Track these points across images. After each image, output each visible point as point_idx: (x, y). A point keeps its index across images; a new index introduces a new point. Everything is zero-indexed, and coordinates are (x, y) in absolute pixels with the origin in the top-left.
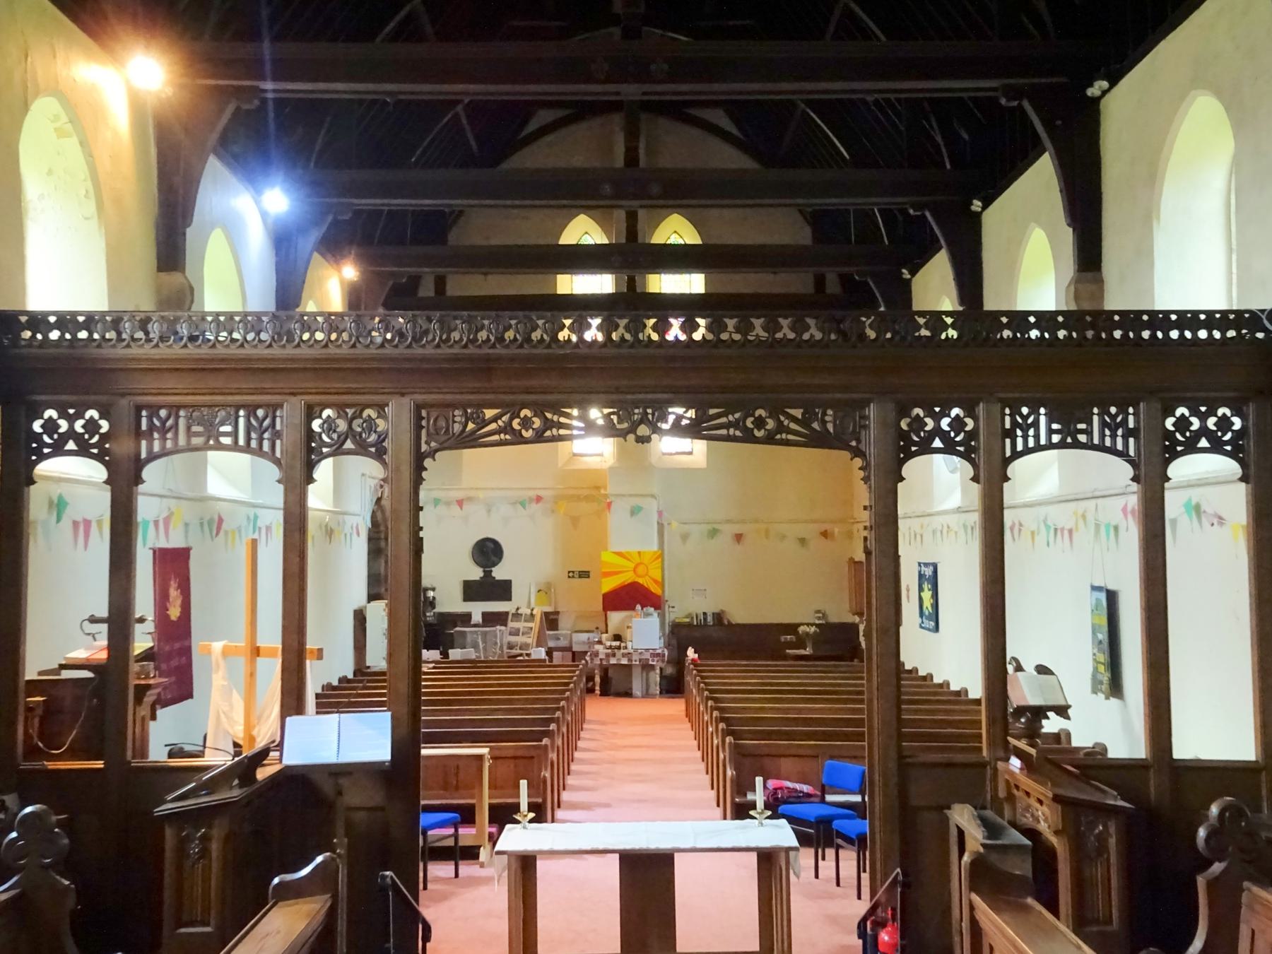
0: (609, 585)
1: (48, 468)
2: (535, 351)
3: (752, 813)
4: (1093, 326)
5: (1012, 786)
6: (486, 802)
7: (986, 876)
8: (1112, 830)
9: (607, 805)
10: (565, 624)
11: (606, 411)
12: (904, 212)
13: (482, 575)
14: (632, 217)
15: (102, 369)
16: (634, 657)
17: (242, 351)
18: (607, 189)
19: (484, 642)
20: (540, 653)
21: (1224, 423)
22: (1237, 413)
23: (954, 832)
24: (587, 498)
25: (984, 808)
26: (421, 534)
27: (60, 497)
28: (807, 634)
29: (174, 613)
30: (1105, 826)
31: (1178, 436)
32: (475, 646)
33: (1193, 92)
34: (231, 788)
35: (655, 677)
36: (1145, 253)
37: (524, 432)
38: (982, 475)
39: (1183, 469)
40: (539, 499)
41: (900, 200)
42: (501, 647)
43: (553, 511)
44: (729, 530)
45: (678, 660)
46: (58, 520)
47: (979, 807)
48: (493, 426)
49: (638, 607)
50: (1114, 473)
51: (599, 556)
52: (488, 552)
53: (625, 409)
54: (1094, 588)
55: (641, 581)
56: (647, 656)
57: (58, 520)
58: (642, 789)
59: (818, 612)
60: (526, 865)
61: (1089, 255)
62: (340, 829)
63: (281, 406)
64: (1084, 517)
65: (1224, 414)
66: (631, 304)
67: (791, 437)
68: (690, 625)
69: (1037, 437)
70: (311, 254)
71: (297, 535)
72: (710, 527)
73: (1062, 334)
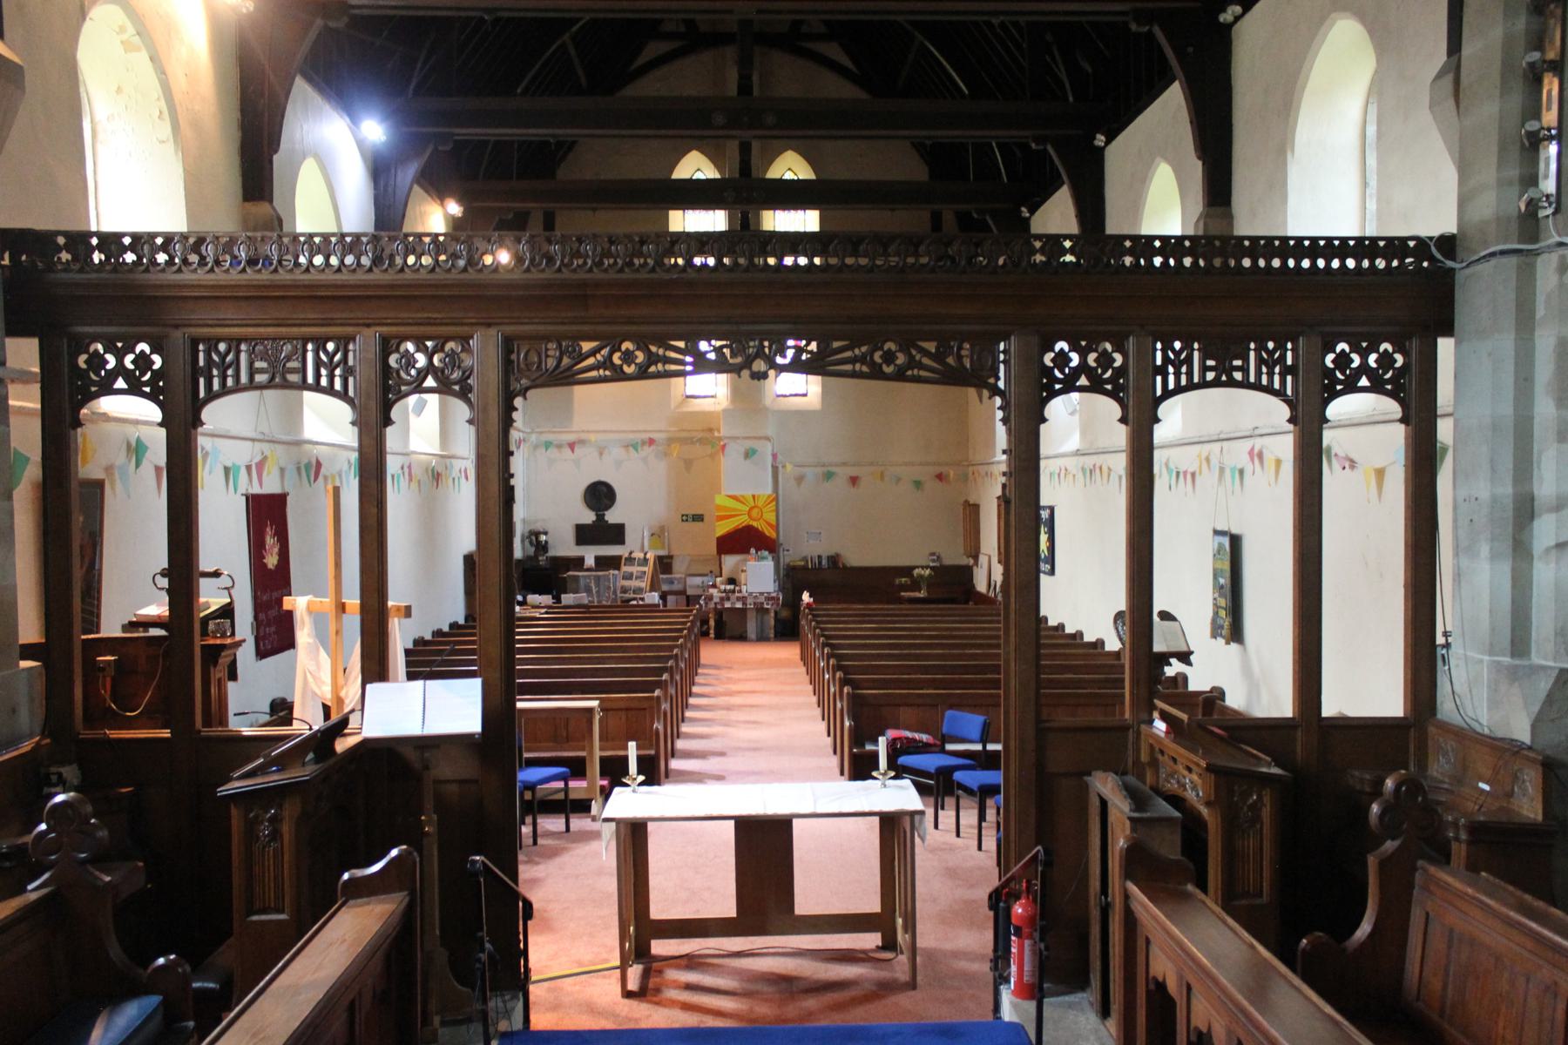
0: (723, 528)
1: (108, 404)
2: (638, 276)
3: (874, 774)
5: (1156, 750)
6: (598, 754)
7: (1140, 863)
8: (1267, 800)
9: (722, 754)
10: (679, 568)
11: (718, 343)
12: (1025, 147)
14: (745, 149)
15: (150, 298)
17: (306, 277)
18: (719, 119)
19: (598, 585)
20: (653, 598)
22: (1400, 348)
23: (1095, 803)
24: (701, 441)
25: (1124, 773)
26: (513, 482)
27: (138, 440)
28: (921, 576)
29: (272, 561)
30: (1260, 797)
32: (588, 590)
33: (1333, 15)
34: (304, 764)
35: (771, 621)
36: (1278, 185)
37: (625, 368)
38: (1131, 416)
39: (1340, 408)
40: (651, 442)
41: (1022, 133)
42: (615, 592)
43: (666, 454)
44: (844, 473)
45: (793, 602)
46: (137, 466)
47: (1121, 772)
48: (591, 361)
49: (753, 551)
50: (1267, 413)
52: (600, 495)
53: (739, 341)
54: (1217, 533)
55: (755, 524)
56: (762, 599)
57: (137, 466)
58: (761, 751)
60: (634, 834)
61: (1218, 189)
62: (429, 804)
63: (354, 339)
64: (1208, 460)
66: (745, 237)
67: (923, 373)
68: (805, 568)
69: (1190, 374)
70: (411, 188)
71: (373, 484)
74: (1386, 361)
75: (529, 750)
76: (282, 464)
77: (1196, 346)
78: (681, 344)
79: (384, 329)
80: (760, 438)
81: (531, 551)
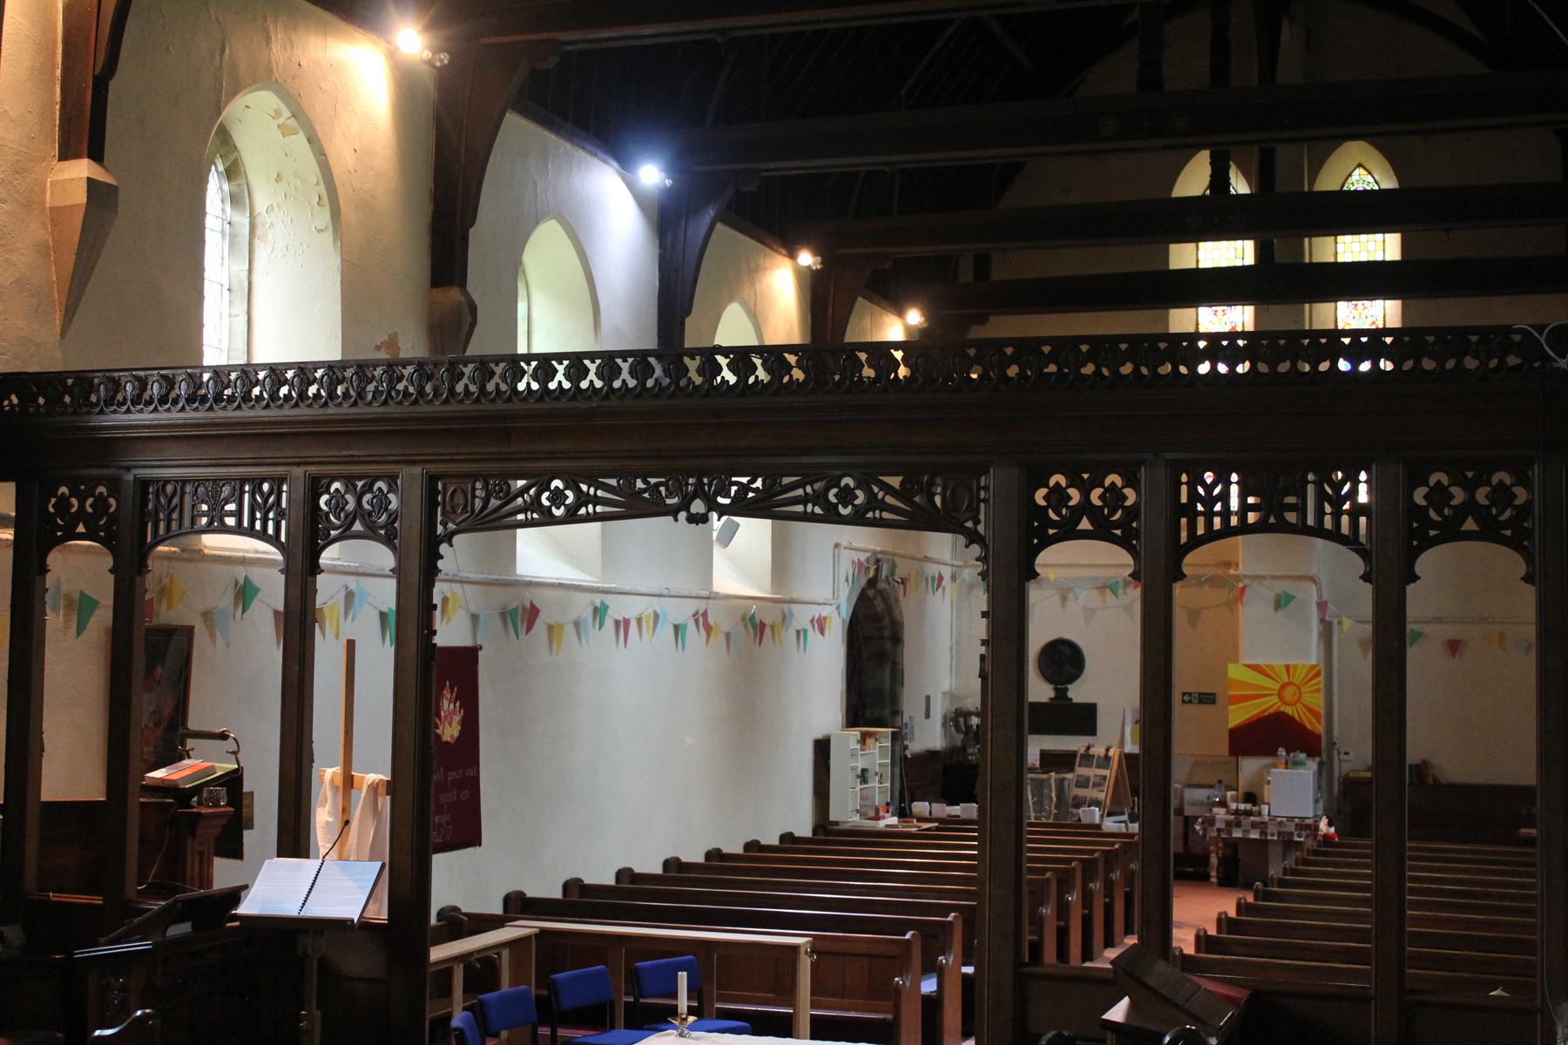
0: (1238, 715)
4: (1130, 356)
13: (1052, 694)
21: (1502, 495)
27: (246, 578)
29: (450, 731)
31: (1433, 514)
49: (1282, 752)
51: (1225, 671)
55: (1289, 710)
56: (1291, 828)
65: (1439, 483)
67: (886, 515)
73: (1127, 369)
74: (1502, 495)
75: (721, 999)
76: (473, 608)
77: (1234, 477)
78: (613, 482)
79: (312, 469)
80: (1299, 578)
81: (959, 739)
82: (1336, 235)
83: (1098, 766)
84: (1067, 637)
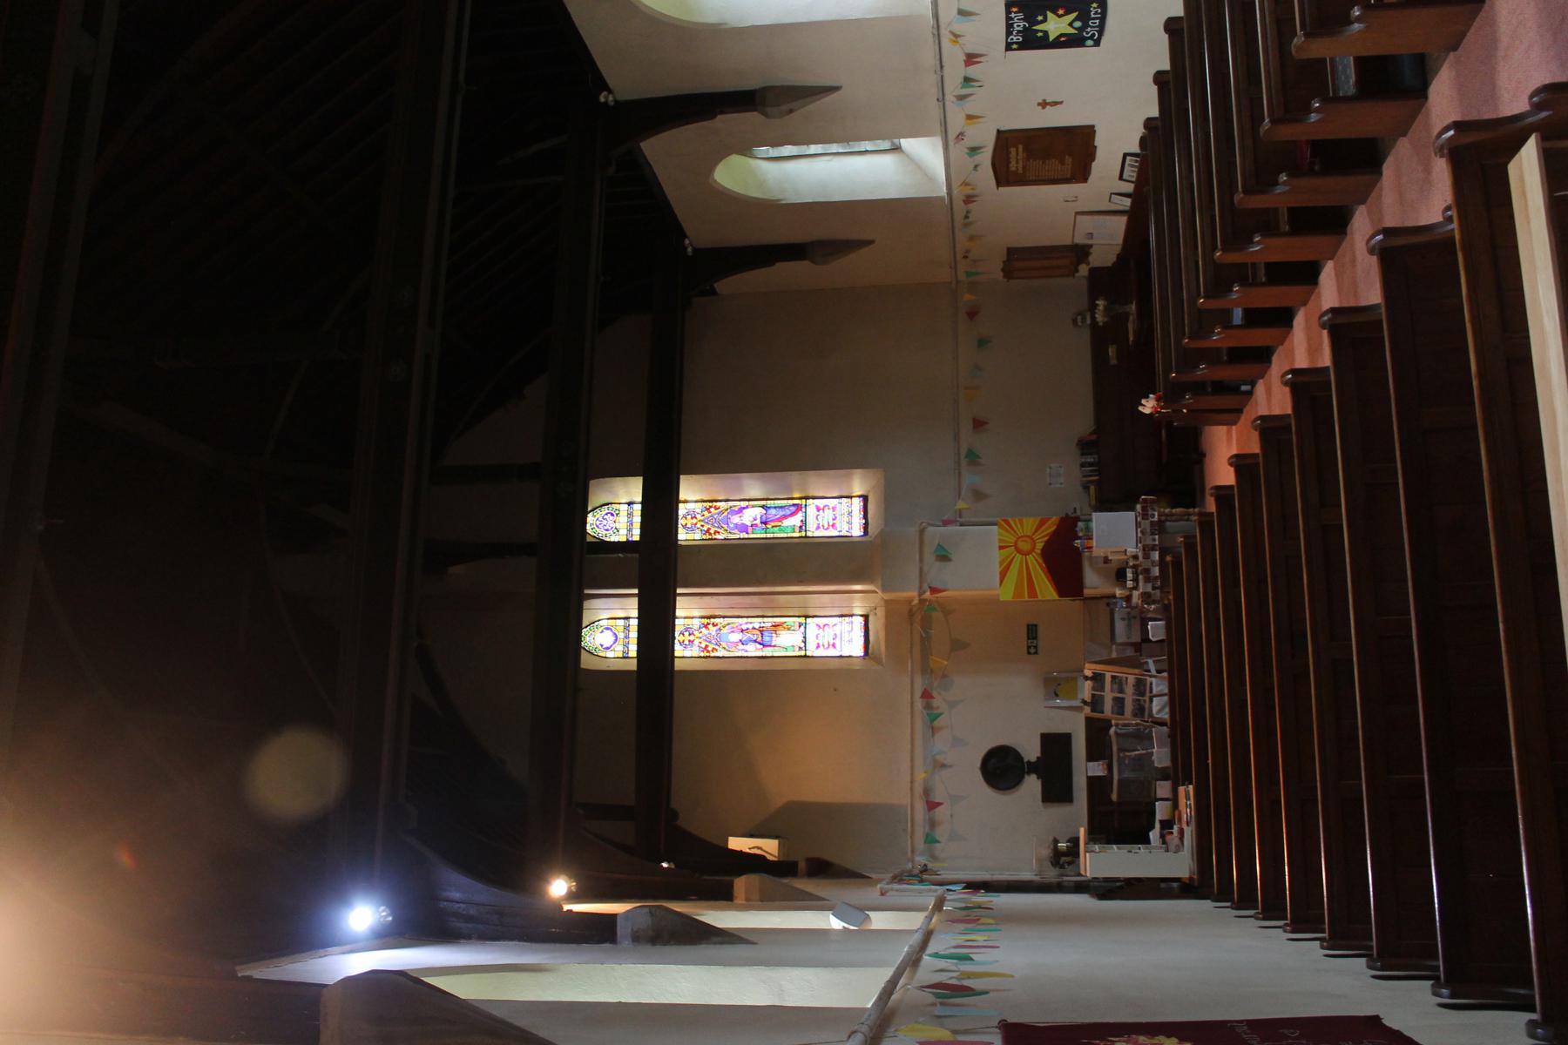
0: (1046, 590)
13: (1034, 777)
16: (1149, 542)
24: (927, 623)
40: (926, 695)
49: (1078, 543)
52: (1001, 768)
55: (1040, 546)
56: (1146, 524)
59: (1075, 321)
72: (964, 462)
82: (673, 657)
83: (1102, 689)
84: (979, 764)
